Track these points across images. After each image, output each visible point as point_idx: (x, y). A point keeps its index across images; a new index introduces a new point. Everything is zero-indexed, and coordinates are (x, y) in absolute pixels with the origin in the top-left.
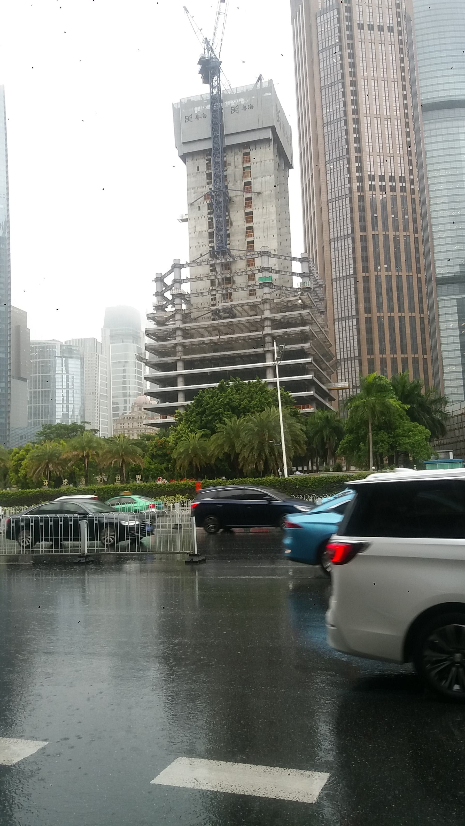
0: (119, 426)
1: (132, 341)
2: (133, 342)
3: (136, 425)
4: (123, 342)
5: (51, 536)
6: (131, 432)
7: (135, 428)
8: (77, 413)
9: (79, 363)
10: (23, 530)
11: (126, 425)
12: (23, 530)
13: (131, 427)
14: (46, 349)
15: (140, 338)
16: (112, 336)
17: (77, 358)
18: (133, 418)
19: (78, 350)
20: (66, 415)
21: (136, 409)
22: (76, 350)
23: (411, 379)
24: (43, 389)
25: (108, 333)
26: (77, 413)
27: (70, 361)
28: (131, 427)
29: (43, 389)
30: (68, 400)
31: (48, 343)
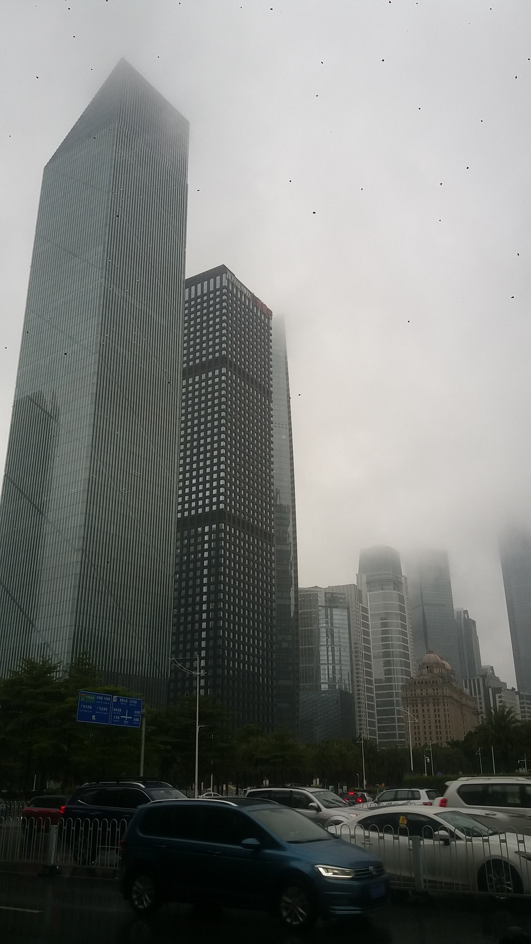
0: (409, 694)
1: (392, 587)
2: (394, 590)
3: (430, 691)
4: (382, 589)
5: (42, 835)
6: (425, 701)
7: (430, 696)
8: (345, 677)
9: (346, 614)
10: (43, 832)
11: (418, 691)
12: (43, 832)
13: (424, 694)
14: (311, 595)
15: (402, 583)
16: (368, 583)
17: (343, 608)
18: (426, 682)
19: (344, 599)
20: (332, 681)
21: (425, 671)
22: (341, 598)
23: (351, 692)
24: (307, 647)
25: (364, 579)
26: (345, 677)
27: (336, 612)
28: (424, 694)
29: (307, 647)
30: (333, 660)
31: (310, 591)
